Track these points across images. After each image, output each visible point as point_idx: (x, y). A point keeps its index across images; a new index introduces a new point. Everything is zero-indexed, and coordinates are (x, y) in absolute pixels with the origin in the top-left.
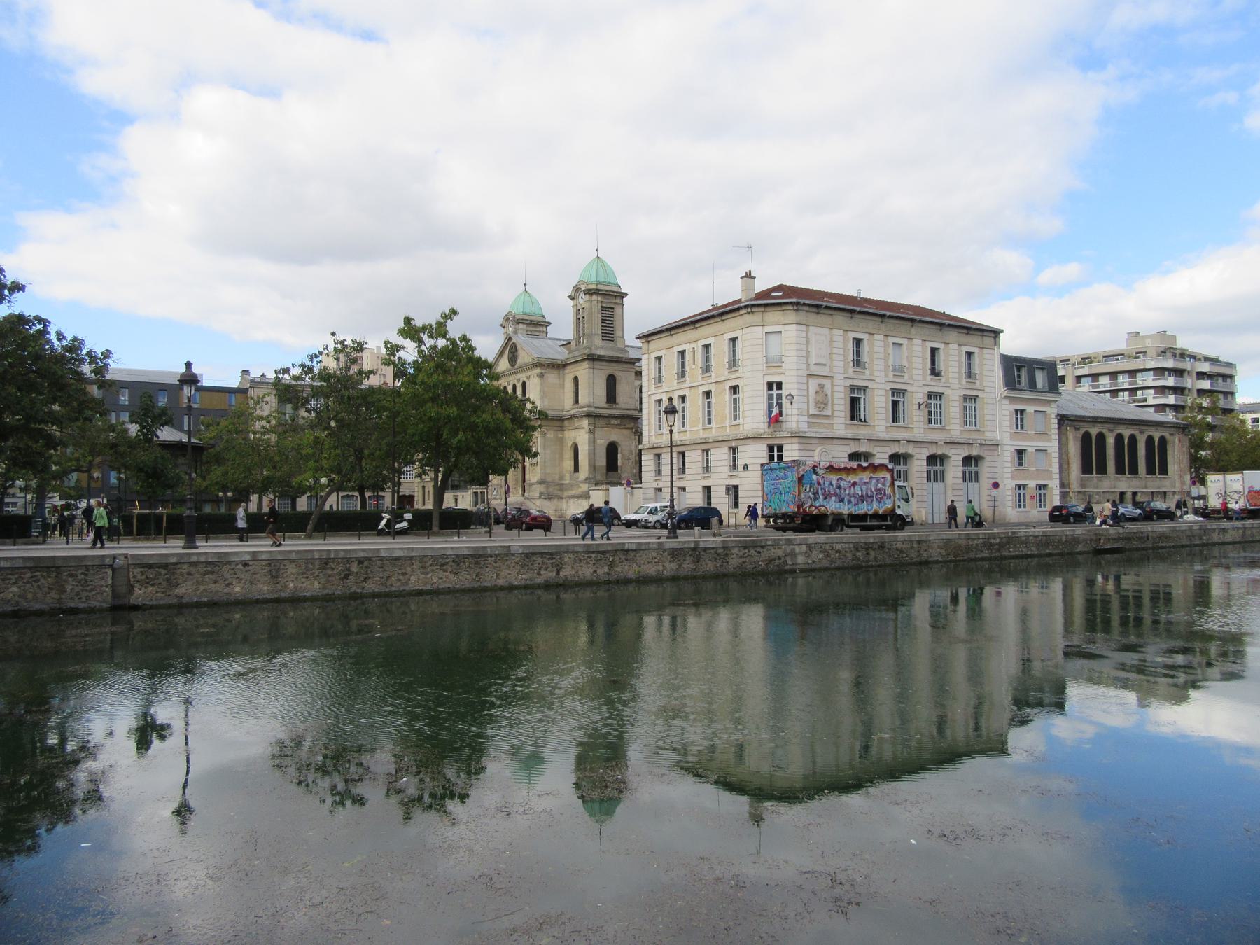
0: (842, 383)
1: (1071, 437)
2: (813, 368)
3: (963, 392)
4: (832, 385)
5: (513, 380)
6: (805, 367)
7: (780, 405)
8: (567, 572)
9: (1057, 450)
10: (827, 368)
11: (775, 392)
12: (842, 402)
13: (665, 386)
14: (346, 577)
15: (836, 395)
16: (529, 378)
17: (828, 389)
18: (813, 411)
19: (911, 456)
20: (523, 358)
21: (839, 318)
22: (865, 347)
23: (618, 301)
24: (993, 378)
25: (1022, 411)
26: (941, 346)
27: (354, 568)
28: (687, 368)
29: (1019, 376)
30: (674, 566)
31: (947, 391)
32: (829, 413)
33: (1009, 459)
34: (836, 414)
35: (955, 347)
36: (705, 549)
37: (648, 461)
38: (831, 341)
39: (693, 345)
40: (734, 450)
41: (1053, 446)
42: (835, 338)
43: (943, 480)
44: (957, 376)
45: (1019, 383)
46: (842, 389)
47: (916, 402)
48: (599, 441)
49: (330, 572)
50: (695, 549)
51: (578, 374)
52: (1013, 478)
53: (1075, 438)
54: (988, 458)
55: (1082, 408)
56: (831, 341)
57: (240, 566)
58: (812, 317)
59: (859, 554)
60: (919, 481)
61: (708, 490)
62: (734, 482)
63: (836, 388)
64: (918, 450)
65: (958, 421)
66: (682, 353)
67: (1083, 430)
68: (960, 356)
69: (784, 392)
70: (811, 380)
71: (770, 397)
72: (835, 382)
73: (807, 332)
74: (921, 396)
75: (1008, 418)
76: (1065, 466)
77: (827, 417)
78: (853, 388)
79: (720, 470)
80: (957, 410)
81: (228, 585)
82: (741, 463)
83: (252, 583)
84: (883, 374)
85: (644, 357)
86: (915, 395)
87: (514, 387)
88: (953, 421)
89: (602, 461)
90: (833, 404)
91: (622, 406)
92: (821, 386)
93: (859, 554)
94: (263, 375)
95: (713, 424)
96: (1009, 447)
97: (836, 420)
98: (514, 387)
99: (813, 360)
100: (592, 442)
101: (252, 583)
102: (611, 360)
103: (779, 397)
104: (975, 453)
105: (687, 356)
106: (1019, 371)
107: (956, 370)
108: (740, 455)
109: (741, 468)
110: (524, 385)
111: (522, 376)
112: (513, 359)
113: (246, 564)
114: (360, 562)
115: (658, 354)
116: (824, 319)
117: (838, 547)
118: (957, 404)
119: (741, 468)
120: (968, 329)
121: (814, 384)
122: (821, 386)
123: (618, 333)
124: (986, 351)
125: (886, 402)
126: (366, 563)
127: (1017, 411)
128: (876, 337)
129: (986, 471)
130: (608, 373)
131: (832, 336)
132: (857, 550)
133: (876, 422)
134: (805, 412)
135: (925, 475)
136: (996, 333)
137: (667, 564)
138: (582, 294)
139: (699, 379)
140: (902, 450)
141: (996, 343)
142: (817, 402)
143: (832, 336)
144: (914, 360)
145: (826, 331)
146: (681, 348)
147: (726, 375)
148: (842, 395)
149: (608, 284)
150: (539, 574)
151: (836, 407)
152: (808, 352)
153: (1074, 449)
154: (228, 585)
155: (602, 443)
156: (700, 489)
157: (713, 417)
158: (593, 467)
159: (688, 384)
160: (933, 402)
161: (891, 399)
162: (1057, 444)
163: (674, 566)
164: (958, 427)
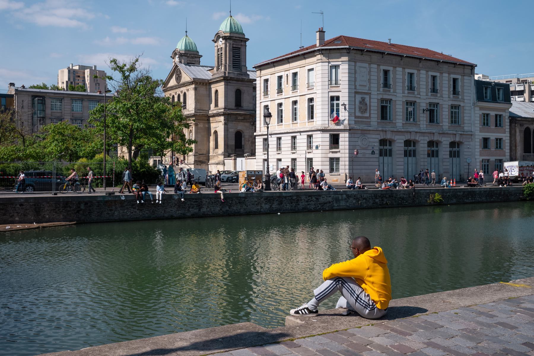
0: (376, 97)
1: (518, 130)
2: (358, 87)
3: (451, 103)
4: (370, 98)
5: (178, 91)
6: (353, 87)
7: (338, 110)
8: (204, 210)
9: (508, 138)
10: (367, 88)
11: (335, 102)
12: (376, 108)
13: (270, 97)
14: (78, 212)
15: (372, 104)
16: (188, 90)
17: (367, 100)
18: (358, 114)
19: (418, 141)
20: (185, 78)
21: (375, 57)
22: (391, 75)
23: (243, 43)
24: (469, 93)
25: (488, 115)
26: (437, 74)
27: (82, 207)
28: (283, 86)
29: (486, 93)
30: (267, 206)
31: (441, 102)
32: (367, 115)
33: (478, 144)
34: (372, 115)
35: (447, 75)
36: (285, 197)
37: (259, 142)
38: (370, 72)
39: (287, 73)
40: (310, 137)
41: (506, 137)
42: (372, 70)
43: (437, 156)
44: (447, 93)
45: (486, 97)
46: (376, 101)
47: (422, 108)
48: (230, 130)
49: (69, 209)
50: (279, 197)
51: (218, 88)
52: (481, 155)
53: (520, 131)
54: (466, 143)
55: (526, 112)
56: (370, 72)
57: (18, 206)
58: (358, 56)
59: (377, 200)
60: (422, 156)
61: (294, 160)
62: (309, 156)
63: (372, 100)
64: (422, 138)
65: (447, 120)
66: (280, 78)
67: (525, 126)
68: (449, 81)
69: (341, 102)
70: (357, 96)
71: (332, 105)
72: (372, 96)
73: (355, 66)
74: (425, 105)
75: (478, 119)
76: (514, 148)
77: (366, 118)
78: (382, 100)
79: (301, 148)
80: (447, 113)
81: (11, 217)
82: (314, 144)
83: (25, 215)
84: (376, 89)
85: (258, 79)
86: (422, 104)
87: (179, 96)
88: (444, 120)
89: (232, 142)
90: (370, 110)
91: (245, 108)
92: (363, 99)
93: (377, 200)
94: (23, 87)
95: (298, 121)
96: (479, 136)
97: (372, 119)
98: (179, 96)
99: (358, 83)
100: (226, 130)
101: (25, 215)
102: (238, 80)
103: (338, 105)
104: (457, 139)
105: (284, 80)
106: (486, 89)
107: (447, 89)
108: (314, 140)
109: (314, 148)
110: (185, 95)
111: (184, 89)
112: (179, 78)
113: (21, 205)
114: (86, 204)
115: (266, 78)
116: (366, 57)
117: (365, 196)
118: (447, 110)
119: (314, 148)
120: (464, 65)
121: (358, 98)
122: (363, 99)
123: (243, 64)
124: (465, 77)
125: (378, 107)
126: (89, 204)
127: (484, 114)
128: (421, 71)
129: (464, 150)
130: (236, 88)
131: (370, 68)
132: (376, 198)
133: (397, 121)
134: (353, 115)
135: (403, 152)
136: (472, 67)
137: (263, 205)
138: (221, 39)
139: (290, 94)
140: (412, 137)
141: (472, 73)
142: (360, 108)
143: (370, 68)
144: (421, 83)
145: (367, 65)
146: (280, 74)
147: (306, 91)
148: (376, 104)
149: (237, 33)
150: (189, 211)
151: (372, 112)
152: (355, 78)
153: (519, 137)
154: (11, 217)
155: (232, 131)
156: (290, 160)
157: (298, 116)
158: (226, 145)
159: (283, 96)
160: (454, 110)
161: (380, 105)
162: (509, 135)
163: (267, 206)
164: (447, 124)
